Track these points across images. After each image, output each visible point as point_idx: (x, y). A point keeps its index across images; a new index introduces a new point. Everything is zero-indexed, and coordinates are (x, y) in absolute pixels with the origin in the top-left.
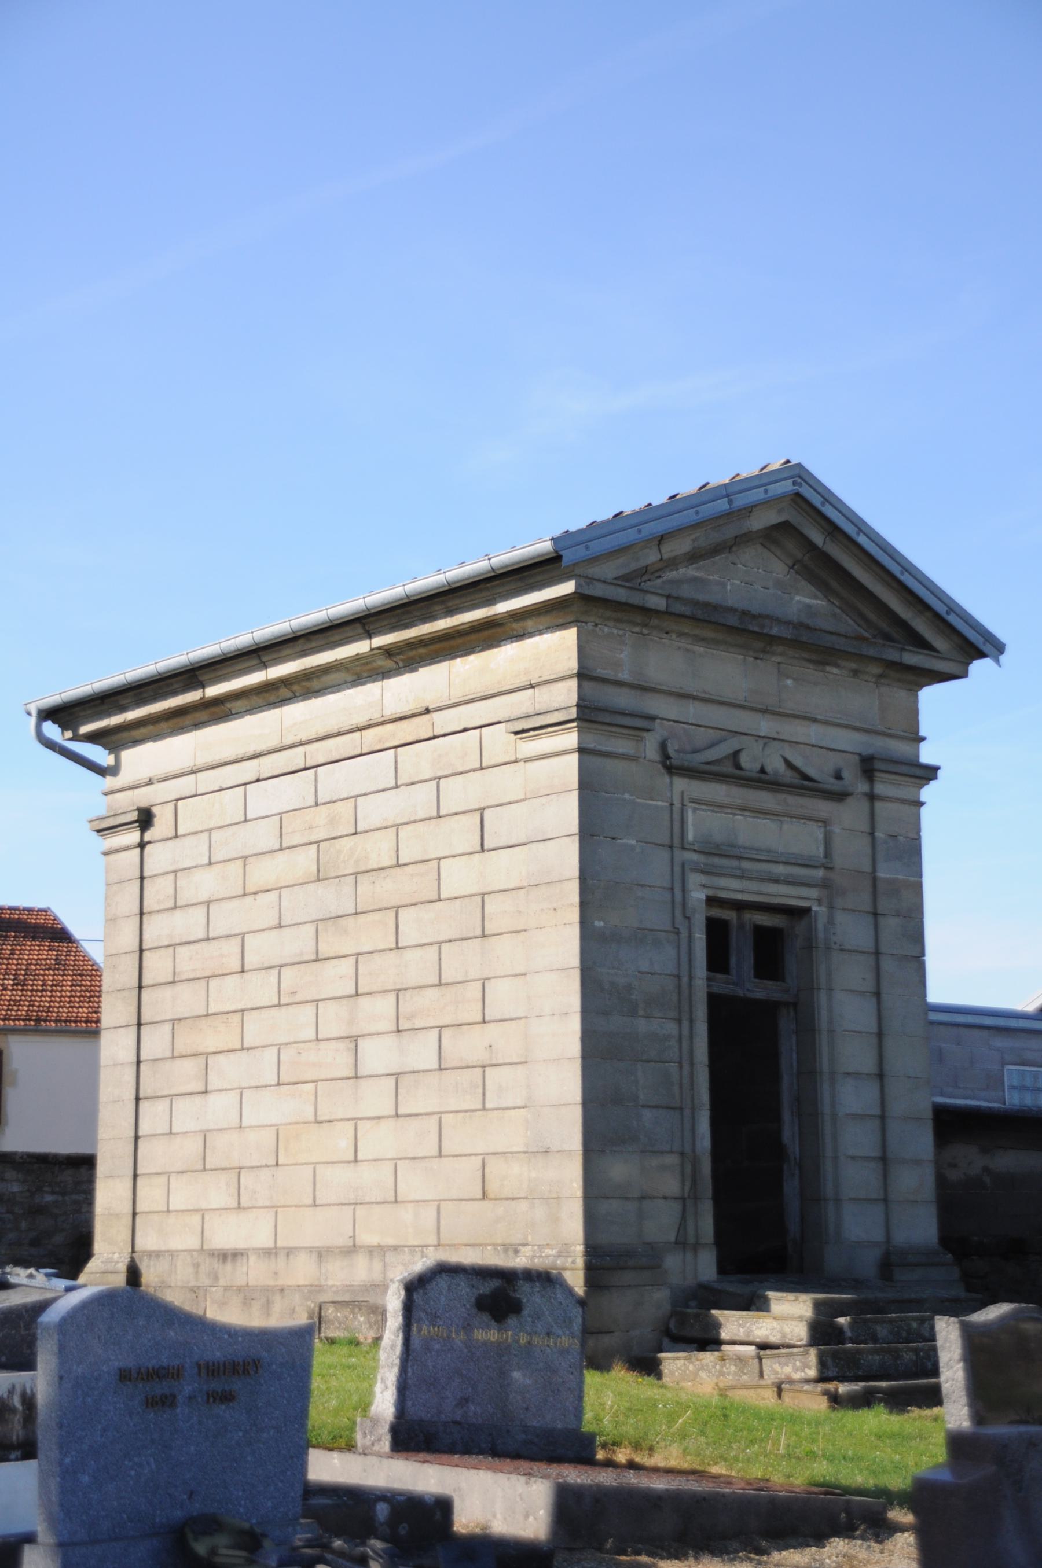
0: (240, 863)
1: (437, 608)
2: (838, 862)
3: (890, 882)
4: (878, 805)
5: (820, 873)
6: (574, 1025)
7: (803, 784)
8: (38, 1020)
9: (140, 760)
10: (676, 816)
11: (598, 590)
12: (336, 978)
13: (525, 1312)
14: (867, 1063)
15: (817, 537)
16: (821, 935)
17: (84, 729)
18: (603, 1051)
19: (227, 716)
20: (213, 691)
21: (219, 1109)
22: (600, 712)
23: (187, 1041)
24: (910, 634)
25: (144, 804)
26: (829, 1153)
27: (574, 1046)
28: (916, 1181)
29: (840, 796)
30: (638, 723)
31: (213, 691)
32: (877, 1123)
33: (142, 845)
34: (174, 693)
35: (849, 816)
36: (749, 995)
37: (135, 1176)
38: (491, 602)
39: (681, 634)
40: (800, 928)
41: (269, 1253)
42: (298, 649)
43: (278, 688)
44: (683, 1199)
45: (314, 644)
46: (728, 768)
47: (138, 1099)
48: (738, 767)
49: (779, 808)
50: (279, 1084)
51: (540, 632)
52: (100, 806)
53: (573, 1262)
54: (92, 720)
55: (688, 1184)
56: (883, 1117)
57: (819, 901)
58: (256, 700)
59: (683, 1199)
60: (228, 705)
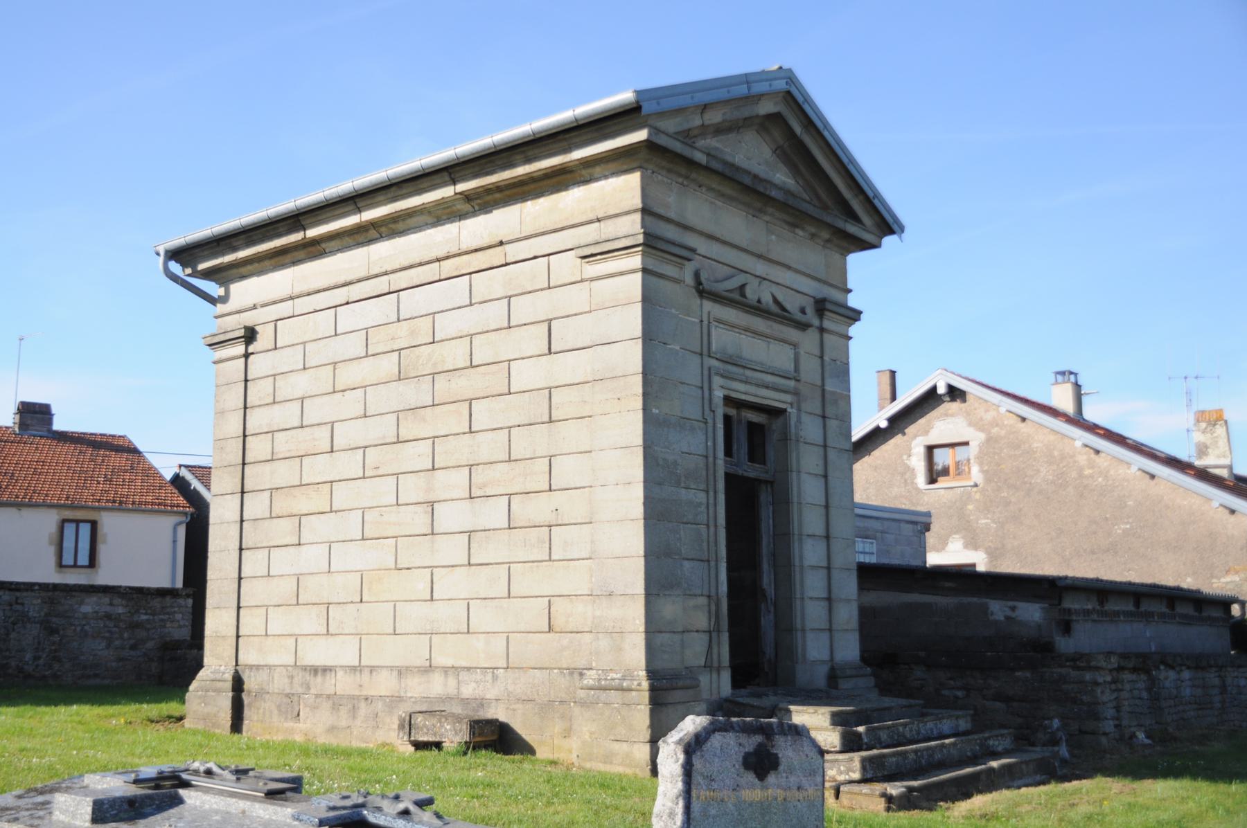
0: (331, 367)
1: (518, 157)
2: (804, 376)
3: (833, 393)
4: (826, 336)
5: (792, 383)
6: (638, 492)
7: (779, 314)
8: (121, 503)
9: (245, 291)
10: (705, 331)
11: (663, 141)
12: (417, 456)
13: (781, 768)
14: (819, 529)
15: (798, 129)
16: (793, 430)
17: (202, 266)
18: (659, 514)
19: (322, 254)
20: (312, 233)
21: (312, 557)
22: (660, 243)
23: (283, 504)
24: (846, 211)
25: (250, 324)
26: (798, 596)
27: (638, 510)
28: (847, 615)
29: (803, 326)
30: (683, 254)
31: (312, 233)
32: (825, 572)
33: (247, 356)
34: (280, 235)
35: (808, 341)
36: (746, 474)
37: (239, 608)
38: (568, 150)
39: (710, 189)
40: (777, 424)
41: (353, 669)
42: (390, 195)
43: (367, 231)
44: (710, 632)
45: (404, 191)
46: (736, 296)
47: (241, 549)
48: (744, 295)
49: (768, 331)
50: (363, 539)
51: (606, 177)
52: (213, 327)
53: (639, 685)
54: (204, 260)
55: (713, 620)
56: (829, 568)
57: (791, 404)
58: (348, 240)
59: (710, 632)
60: (323, 245)
